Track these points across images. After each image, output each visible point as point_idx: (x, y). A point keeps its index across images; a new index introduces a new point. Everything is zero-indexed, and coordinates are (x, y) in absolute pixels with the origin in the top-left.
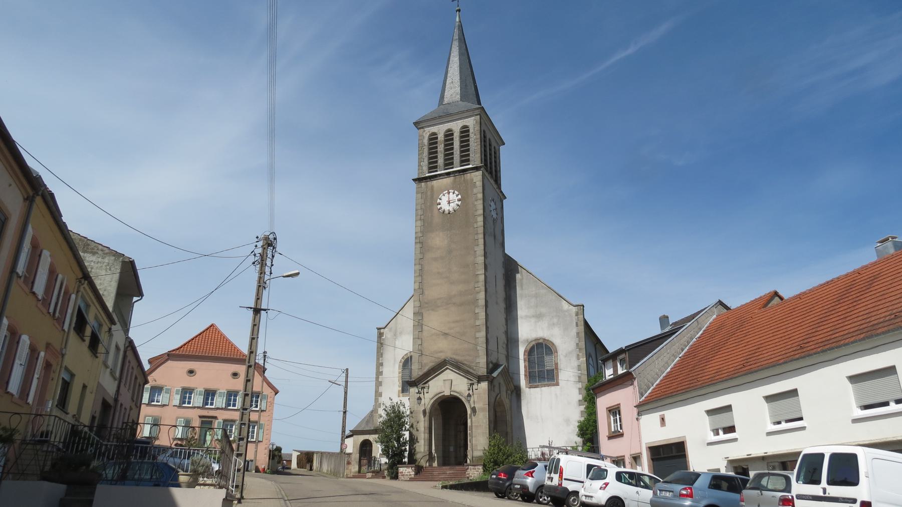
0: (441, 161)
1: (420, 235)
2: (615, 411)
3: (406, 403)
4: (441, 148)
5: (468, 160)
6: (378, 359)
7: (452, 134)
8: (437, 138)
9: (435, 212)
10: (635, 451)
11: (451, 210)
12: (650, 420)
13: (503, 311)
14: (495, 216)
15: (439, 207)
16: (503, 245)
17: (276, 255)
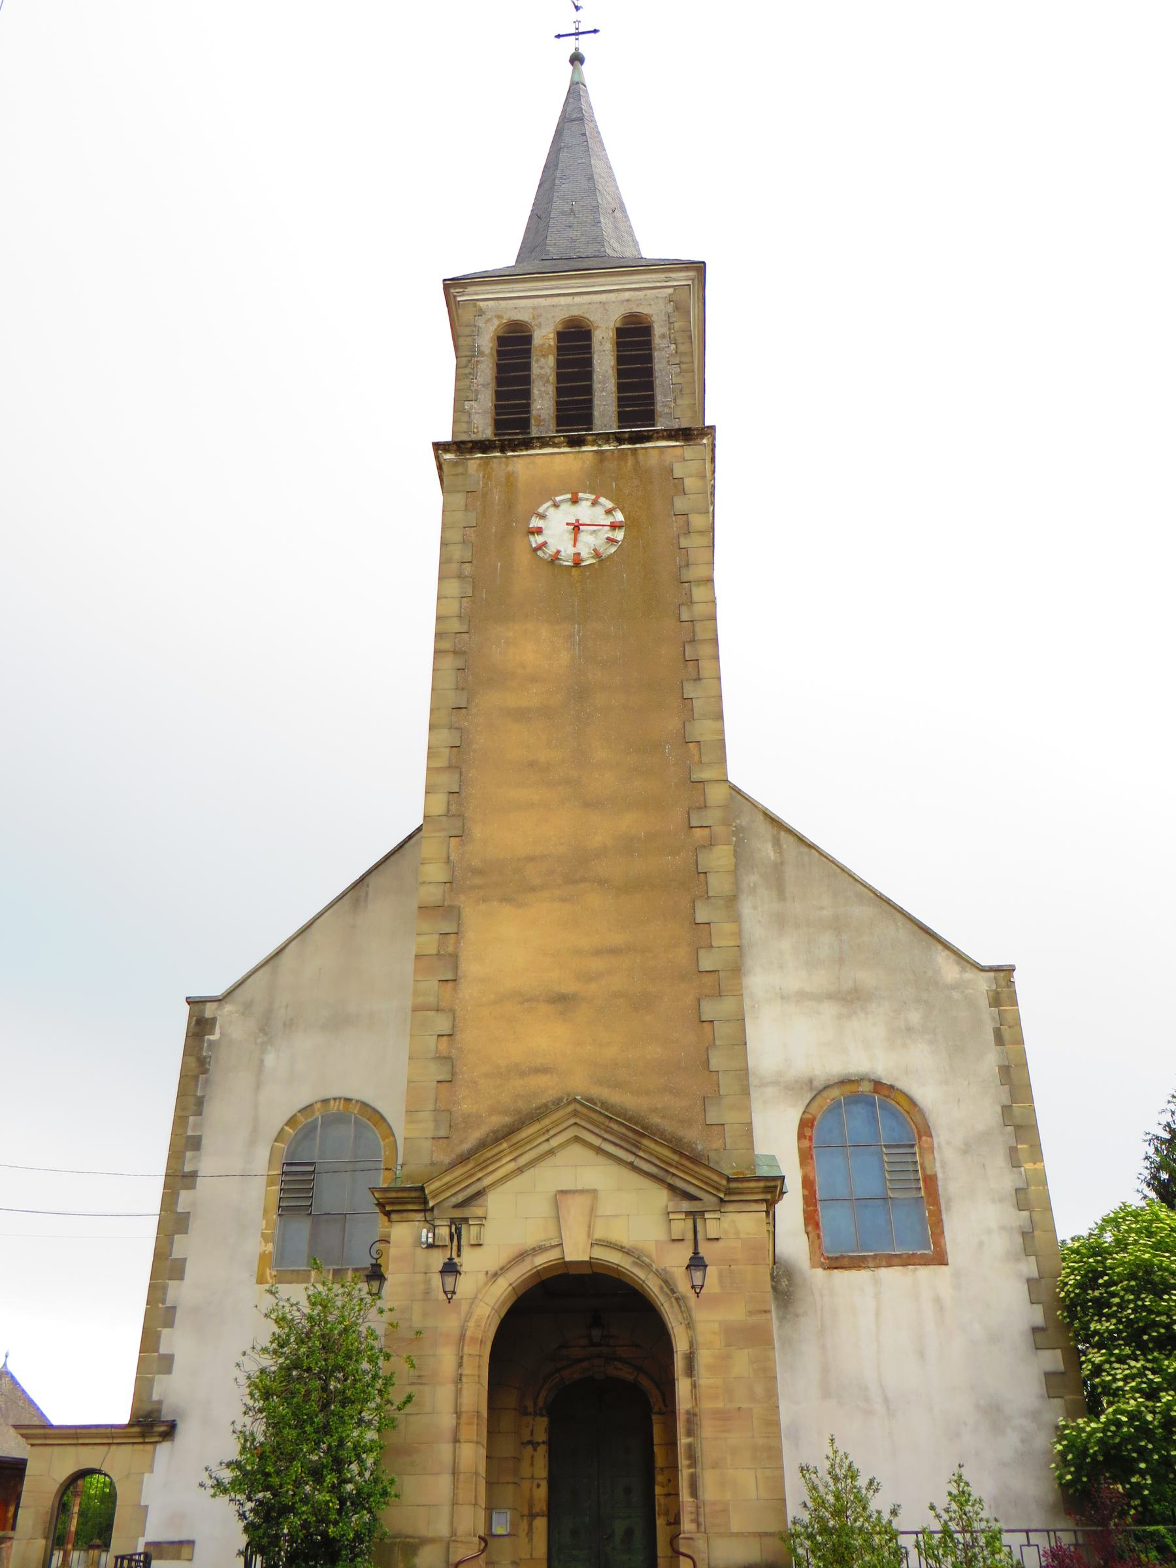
1: (455, 626)
6: (180, 1120)
9: (523, 559)
15: (536, 540)
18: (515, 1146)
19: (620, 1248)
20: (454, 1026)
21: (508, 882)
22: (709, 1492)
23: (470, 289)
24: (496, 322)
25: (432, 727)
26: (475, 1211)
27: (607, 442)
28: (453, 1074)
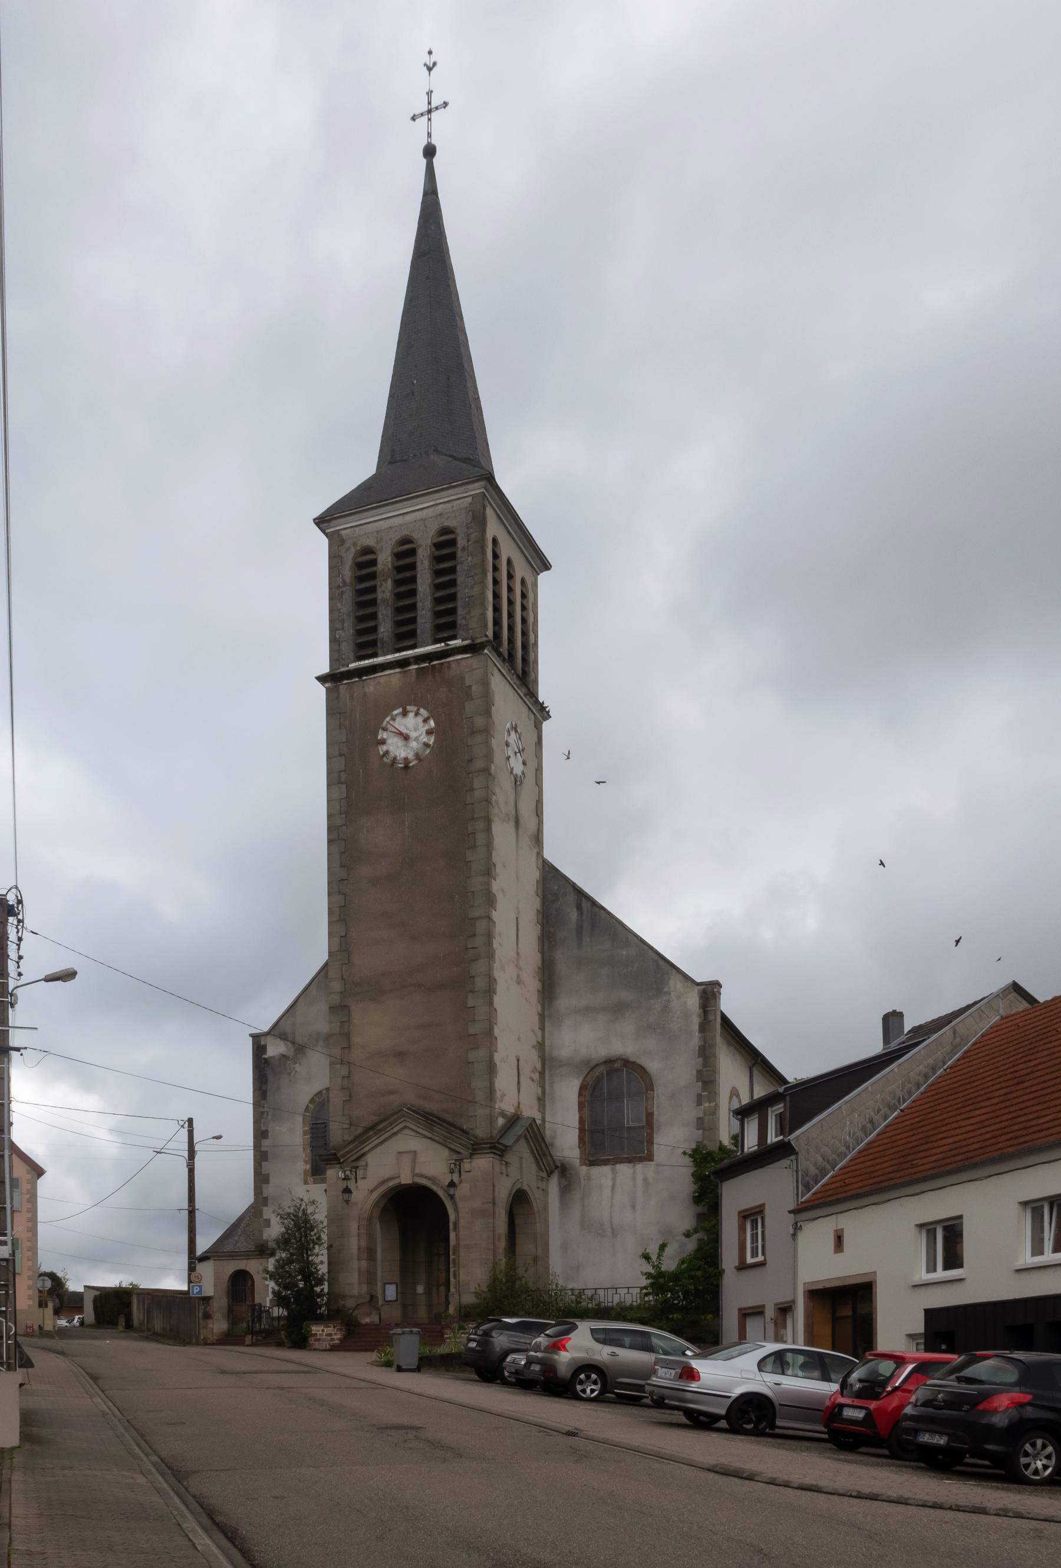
0: (385, 629)
2: (753, 1216)
3: (317, 1200)
4: (385, 589)
5: (453, 625)
7: (413, 552)
8: (374, 563)
10: (784, 1298)
11: (411, 756)
12: (817, 1235)
13: (534, 997)
14: (518, 769)
16: (538, 839)
17: (26, 936)
18: (376, 1134)
19: (426, 1177)
20: (350, 1072)
21: (372, 989)
22: (463, 1276)
23: (333, 523)
24: (353, 550)
25: (329, 894)
26: (362, 1163)
27: (424, 662)
28: (350, 1096)
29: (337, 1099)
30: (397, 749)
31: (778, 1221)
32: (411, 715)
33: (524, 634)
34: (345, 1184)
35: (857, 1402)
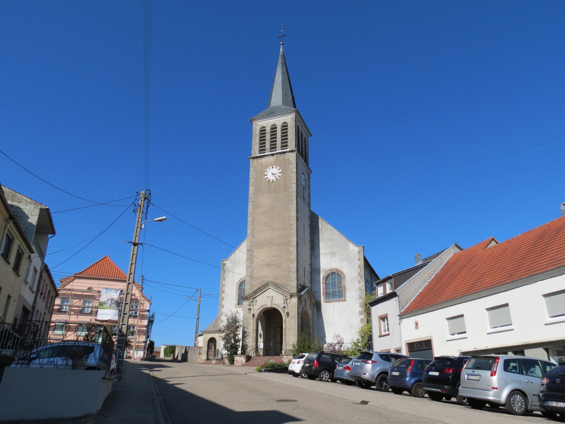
0: (268, 145)
2: (384, 318)
3: (240, 313)
4: (268, 137)
5: (287, 146)
7: (276, 128)
8: (265, 130)
16: (309, 204)
29: (248, 280)
30: (271, 177)
31: (393, 318)
32: (274, 168)
33: (305, 151)
34: (249, 307)
35: (358, 360)
